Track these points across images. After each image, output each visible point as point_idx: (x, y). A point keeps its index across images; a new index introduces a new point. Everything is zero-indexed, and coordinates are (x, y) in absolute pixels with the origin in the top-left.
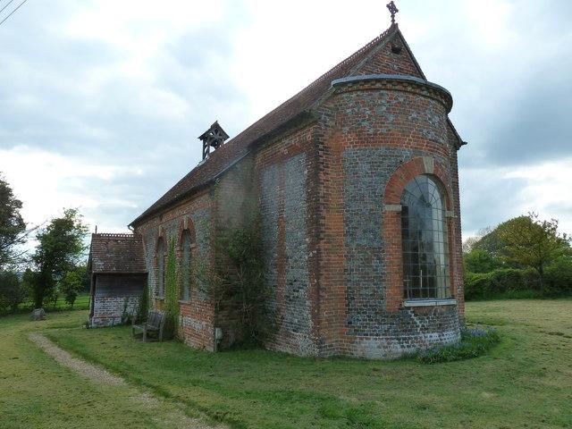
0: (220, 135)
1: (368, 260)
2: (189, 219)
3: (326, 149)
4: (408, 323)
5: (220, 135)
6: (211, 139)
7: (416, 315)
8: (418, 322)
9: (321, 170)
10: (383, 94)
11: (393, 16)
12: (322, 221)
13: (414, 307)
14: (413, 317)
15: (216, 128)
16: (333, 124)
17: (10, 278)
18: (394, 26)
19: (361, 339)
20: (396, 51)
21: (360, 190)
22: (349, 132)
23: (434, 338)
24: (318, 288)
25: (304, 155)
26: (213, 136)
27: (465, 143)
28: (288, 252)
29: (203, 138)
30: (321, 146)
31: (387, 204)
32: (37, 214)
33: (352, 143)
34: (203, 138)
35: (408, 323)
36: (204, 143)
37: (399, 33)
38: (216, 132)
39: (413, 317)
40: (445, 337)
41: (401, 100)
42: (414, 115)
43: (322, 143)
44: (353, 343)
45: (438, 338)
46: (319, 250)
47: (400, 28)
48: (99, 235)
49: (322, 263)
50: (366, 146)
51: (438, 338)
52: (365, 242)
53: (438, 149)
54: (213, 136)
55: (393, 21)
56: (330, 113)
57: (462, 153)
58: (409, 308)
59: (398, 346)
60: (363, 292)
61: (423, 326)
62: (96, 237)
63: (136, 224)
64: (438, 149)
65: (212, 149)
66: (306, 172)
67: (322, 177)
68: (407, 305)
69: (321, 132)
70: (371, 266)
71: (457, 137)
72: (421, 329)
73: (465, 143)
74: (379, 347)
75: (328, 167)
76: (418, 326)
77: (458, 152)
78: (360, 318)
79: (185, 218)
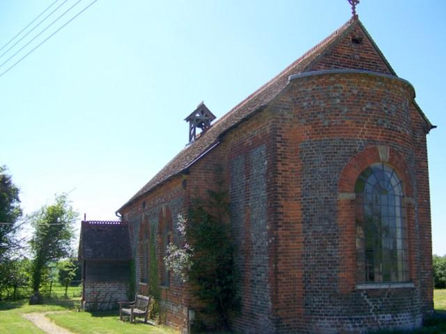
0: (206, 116)
1: (323, 246)
2: (167, 207)
3: (284, 141)
4: (361, 305)
5: (206, 116)
6: (197, 120)
7: (369, 297)
8: (370, 304)
9: (279, 161)
10: (336, 88)
11: (354, 8)
12: (280, 210)
13: (366, 290)
14: (365, 299)
15: (202, 109)
16: (291, 116)
17: (11, 264)
18: (355, 17)
19: (317, 319)
20: (356, 41)
21: (316, 179)
22: (306, 125)
23: (386, 319)
24: (276, 272)
25: (264, 147)
26: (200, 118)
27: (435, 127)
28: (253, 238)
29: (190, 119)
30: (279, 139)
31: (341, 192)
32: (32, 203)
33: (309, 135)
34: (190, 119)
35: (361, 305)
36: (191, 125)
37: (359, 24)
38: (202, 113)
39: (365, 299)
40: (399, 318)
41: (355, 92)
42: (368, 106)
43: (280, 136)
44: (309, 323)
45: (391, 319)
46: (276, 237)
47: (360, 19)
48: (88, 222)
49: (280, 249)
50: (321, 137)
51: (391, 319)
52: (320, 229)
53: (394, 137)
54: (200, 118)
55: (354, 12)
56: (287, 107)
57: (431, 137)
58: (361, 290)
59: (350, 325)
60: (319, 275)
61: (376, 307)
62: (85, 225)
63: (122, 211)
64: (394, 137)
65: (199, 131)
66: (266, 163)
67: (280, 167)
68: (360, 287)
69: (279, 125)
70: (326, 251)
71: (427, 121)
72: (373, 311)
73: (435, 127)
74: (332, 326)
75: (286, 158)
76: (371, 308)
77: (427, 135)
78: (315, 300)
79: (163, 207)
